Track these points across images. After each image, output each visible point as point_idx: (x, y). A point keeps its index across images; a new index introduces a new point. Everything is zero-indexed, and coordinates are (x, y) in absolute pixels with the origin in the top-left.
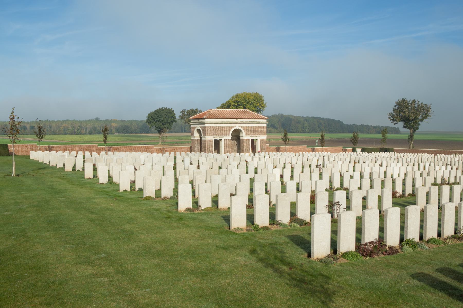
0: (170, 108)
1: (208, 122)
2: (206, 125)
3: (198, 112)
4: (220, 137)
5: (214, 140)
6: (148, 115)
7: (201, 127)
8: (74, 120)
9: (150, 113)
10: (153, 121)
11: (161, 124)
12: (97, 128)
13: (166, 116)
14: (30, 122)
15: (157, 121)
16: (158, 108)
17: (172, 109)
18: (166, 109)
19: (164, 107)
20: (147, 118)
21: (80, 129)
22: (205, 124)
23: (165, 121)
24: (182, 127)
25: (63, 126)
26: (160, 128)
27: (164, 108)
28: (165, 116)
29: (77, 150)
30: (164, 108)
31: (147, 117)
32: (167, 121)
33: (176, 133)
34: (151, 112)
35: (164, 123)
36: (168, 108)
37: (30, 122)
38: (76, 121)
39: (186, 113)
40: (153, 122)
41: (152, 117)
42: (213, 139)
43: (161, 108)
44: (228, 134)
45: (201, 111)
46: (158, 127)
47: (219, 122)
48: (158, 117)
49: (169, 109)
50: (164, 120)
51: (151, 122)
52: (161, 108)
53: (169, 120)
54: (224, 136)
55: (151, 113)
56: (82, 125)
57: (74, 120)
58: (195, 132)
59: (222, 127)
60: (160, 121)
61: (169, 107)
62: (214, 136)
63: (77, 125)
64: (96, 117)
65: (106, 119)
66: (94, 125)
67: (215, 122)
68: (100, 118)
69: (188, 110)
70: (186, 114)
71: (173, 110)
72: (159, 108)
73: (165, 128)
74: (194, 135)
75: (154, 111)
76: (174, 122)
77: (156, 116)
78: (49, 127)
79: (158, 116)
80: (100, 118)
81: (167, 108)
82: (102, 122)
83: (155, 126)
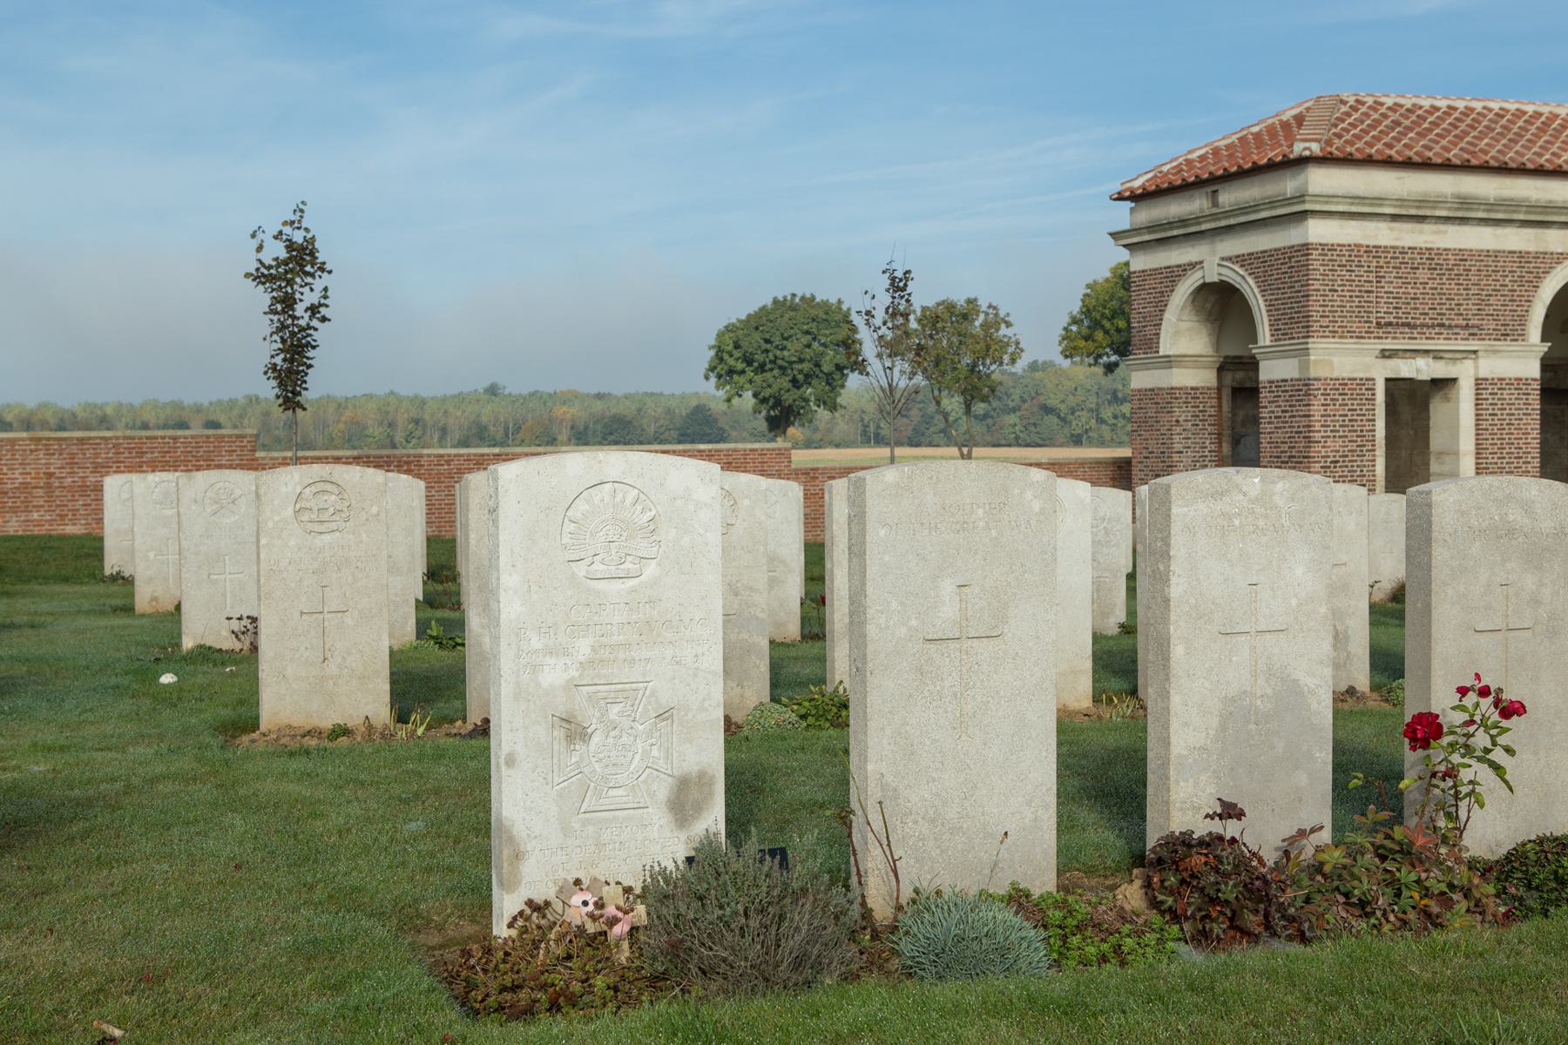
0: (833, 300)
1: (1330, 197)
2: (1318, 231)
3: (978, 315)
4: (1437, 355)
5: (1388, 380)
6: (714, 336)
7: (1240, 260)
8: (392, 393)
9: (725, 324)
10: (740, 366)
11: (785, 383)
12: (491, 427)
13: (809, 337)
14: (206, 403)
15: (762, 368)
16: (769, 302)
17: (840, 302)
18: (809, 301)
19: (800, 295)
20: (712, 353)
21: (418, 433)
22: (1303, 215)
23: (806, 366)
24: (866, 419)
25: (343, 419)
26: (778, 403)
27: (797, 300)
28: (806, 339)
29: (49, 486)
30: (797, 300)
31: (711, 348)
32: (818, 365)
33: (837, 446)
34: (734, 320)
35: (800, 377)
36: (818, 300)
37: (206, 403)
38: (400, 399)
39: (913, 325)
40: (743, 372)
41: (737, 346)
42: (1381, 371)
43: (785, 300)
44: (1511, 331)
45: (995, 308)
46: (771, 402)
47: (1435, 204)
48: (768, 346)
49: (825, 304)
50: (801, 361)
51: (731, 372)
52: (785, 300)
53: (828, 358)
54: (1473, 345)
55: (733, 325)
56: (427, 417)
57: (392, 393)
58: (1170, 316)
59: (1463, 256)
60: (781, 367)
61: (826, 293)
62: (1390, 344)
63: (406, 415)
64: (487, 384)
65: (532, 390)
66: (478, 416)
67: (1401, 201)
68: (504, 387)
69: (924, 309)
70: (916, 330)
71: (844, 307)
72: (776, 301)
73: (807, 401)
74: (1166, 347)
75: (749, 316)
76: (852, 371)
77: (757, 336)
78: (285, 424)
79: (767, 341)
80: (504, 387)
81: (813, 298)
82: (514, 401)
83: (755, 395)
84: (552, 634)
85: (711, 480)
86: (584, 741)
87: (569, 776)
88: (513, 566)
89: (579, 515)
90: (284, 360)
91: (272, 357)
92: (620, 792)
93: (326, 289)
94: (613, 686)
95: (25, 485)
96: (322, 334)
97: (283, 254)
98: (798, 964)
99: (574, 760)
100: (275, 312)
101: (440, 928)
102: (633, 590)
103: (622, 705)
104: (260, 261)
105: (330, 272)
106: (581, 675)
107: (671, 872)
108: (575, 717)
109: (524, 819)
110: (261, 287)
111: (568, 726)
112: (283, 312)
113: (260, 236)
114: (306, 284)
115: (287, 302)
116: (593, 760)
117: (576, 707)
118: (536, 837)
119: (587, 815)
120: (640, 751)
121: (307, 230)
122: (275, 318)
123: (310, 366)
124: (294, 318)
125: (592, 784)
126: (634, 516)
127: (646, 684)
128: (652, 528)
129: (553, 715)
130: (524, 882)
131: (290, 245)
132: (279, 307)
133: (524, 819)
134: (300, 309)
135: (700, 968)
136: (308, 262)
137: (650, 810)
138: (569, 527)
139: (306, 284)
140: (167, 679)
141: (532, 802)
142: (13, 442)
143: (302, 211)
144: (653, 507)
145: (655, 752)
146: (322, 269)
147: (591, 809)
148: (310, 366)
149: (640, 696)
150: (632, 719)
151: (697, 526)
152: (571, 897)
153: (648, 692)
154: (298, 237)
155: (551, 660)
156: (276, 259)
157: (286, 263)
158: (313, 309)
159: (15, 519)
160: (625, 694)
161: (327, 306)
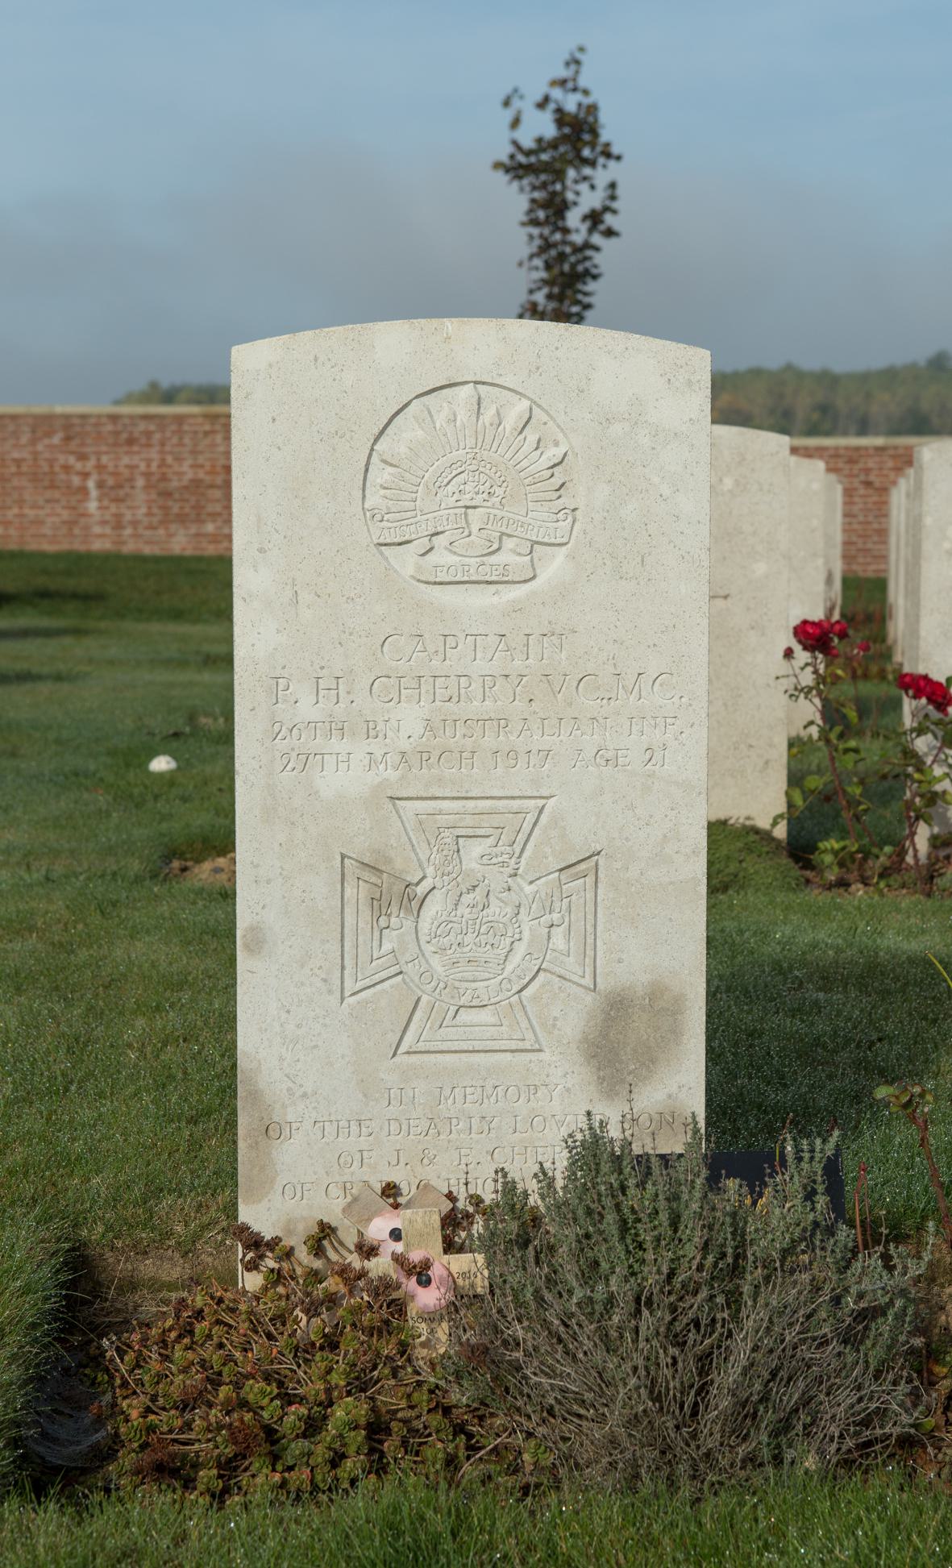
84: (342, 694)
85: (689, 383)
86: (409, 911)
87: (377, 978)
88: (261, 550)
89: (403, 450)
90: (550, 297)
91: (531, 292)
92: (485, 1016)
93: (613, 186)
94: (471, 804)
95: (196, 483)
96: (608, 256)
97: (550, 131)
98: (745, 1414)
99: (387, 946)
100: (535, 222)
101: (187, 1250)
102: (516, 609)
103: (491, 841)
104: (515, 143)
105: (618, 158)
106: (403, 777)
107: (526, 1194)
108: (389, 861)
109: (281, 1059)
110: (515, 184)
111: (374, 879)
112: (547, 222)
113: (516, 104)
114: (585, 178)
115: (554, 208)
116: (428, 949)
117: (393, 841)
118: (305, 1095)
119: (414, 1058)
120: (526, 935)
121: (586, 92)
122: (535, 231)
123: (588, 307)
124: (566, 231)
125: (425, 998)
126: (520, 456)
127: (541, 802)
128: (556, 481)
129: (343, 857)
130: (280, 1181)
131: (561, 117)
132: (541, 214)
133: (281, 1059)
134: (573, 218)
135: (102, 1512)
136: (586, 143)
137: (545, 1056)
138: (380, 475)
139: (585, 178)
140: (161, 764)
141: (299, 1026)
142: (180, 419)
143: (577, 62)
144: (560, 437)
145: (558, 939)
146: (608, 155)
147: (421, 1046)
148: (588, 307)
149: (527, 827)
150: (510, 870)
151: (656, 480)
152: (369, 1220)
153: (544, 819)
154: (571, 103)
155: (337, 745)
156: (539, 140)
157: (554, 145)
158: (594, 218)
159: (182, 532)
160: (496, 820)
161: (614, 212)
